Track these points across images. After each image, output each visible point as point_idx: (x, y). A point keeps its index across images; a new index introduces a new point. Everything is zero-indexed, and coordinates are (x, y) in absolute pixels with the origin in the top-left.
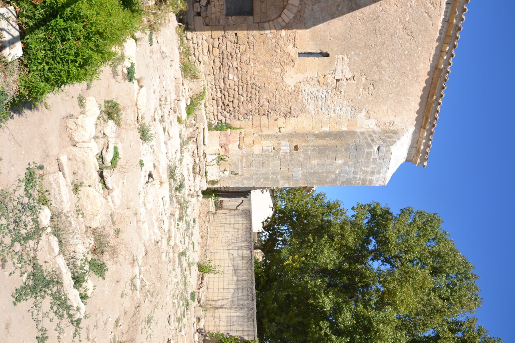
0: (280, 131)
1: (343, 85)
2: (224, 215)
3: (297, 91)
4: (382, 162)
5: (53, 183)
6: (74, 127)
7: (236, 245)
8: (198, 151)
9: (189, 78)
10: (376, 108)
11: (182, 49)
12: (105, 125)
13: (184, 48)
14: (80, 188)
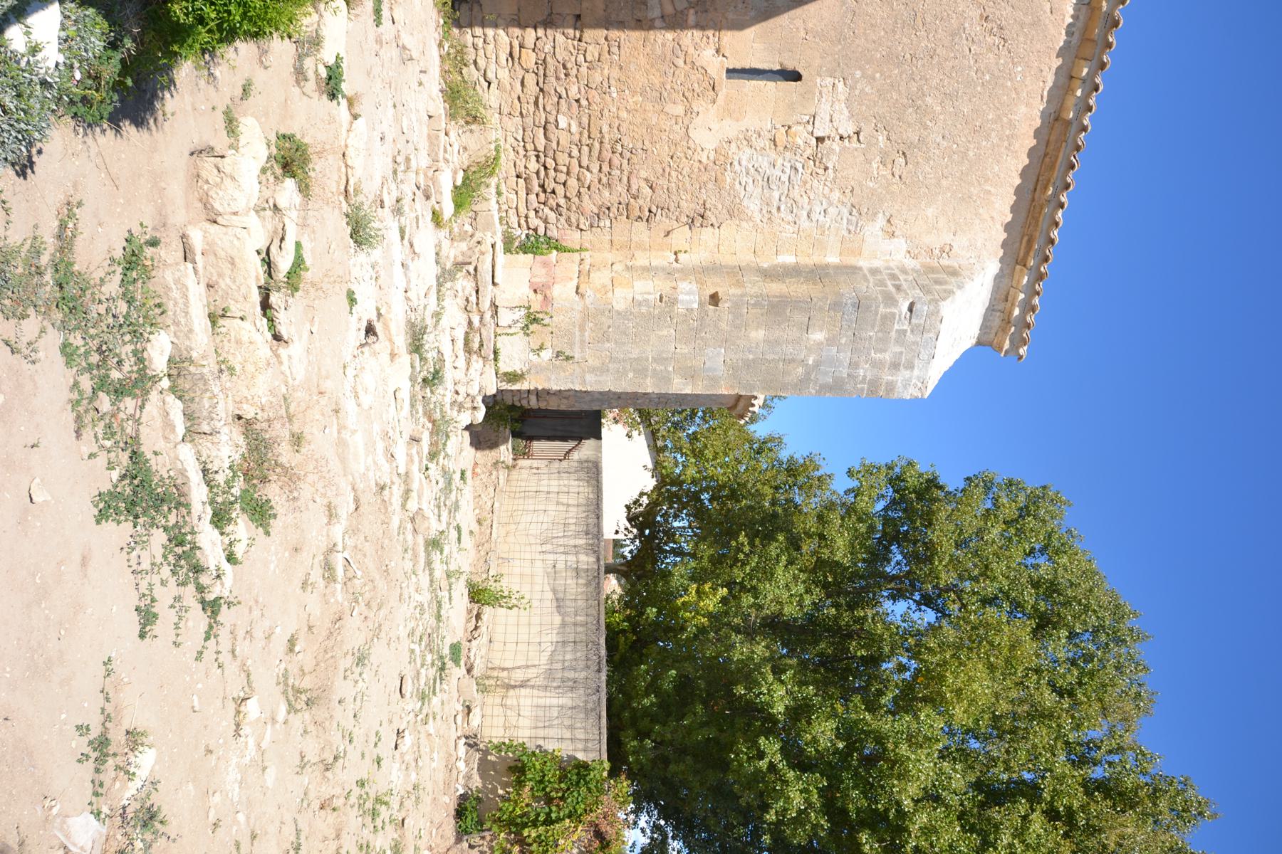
0: (677, 261)
1: (832, 150)
2: (535, 471)
3: (722, 161)
4: (919, 339)
5: (174, 287)
6: (213, 176)
7: (561, 541)
8: (478, 298)
9: (462, 122)
10: (910, 210)
11: (446, 48)
12: (278, 188)
13: (451, 46)
14: (221, 322)
